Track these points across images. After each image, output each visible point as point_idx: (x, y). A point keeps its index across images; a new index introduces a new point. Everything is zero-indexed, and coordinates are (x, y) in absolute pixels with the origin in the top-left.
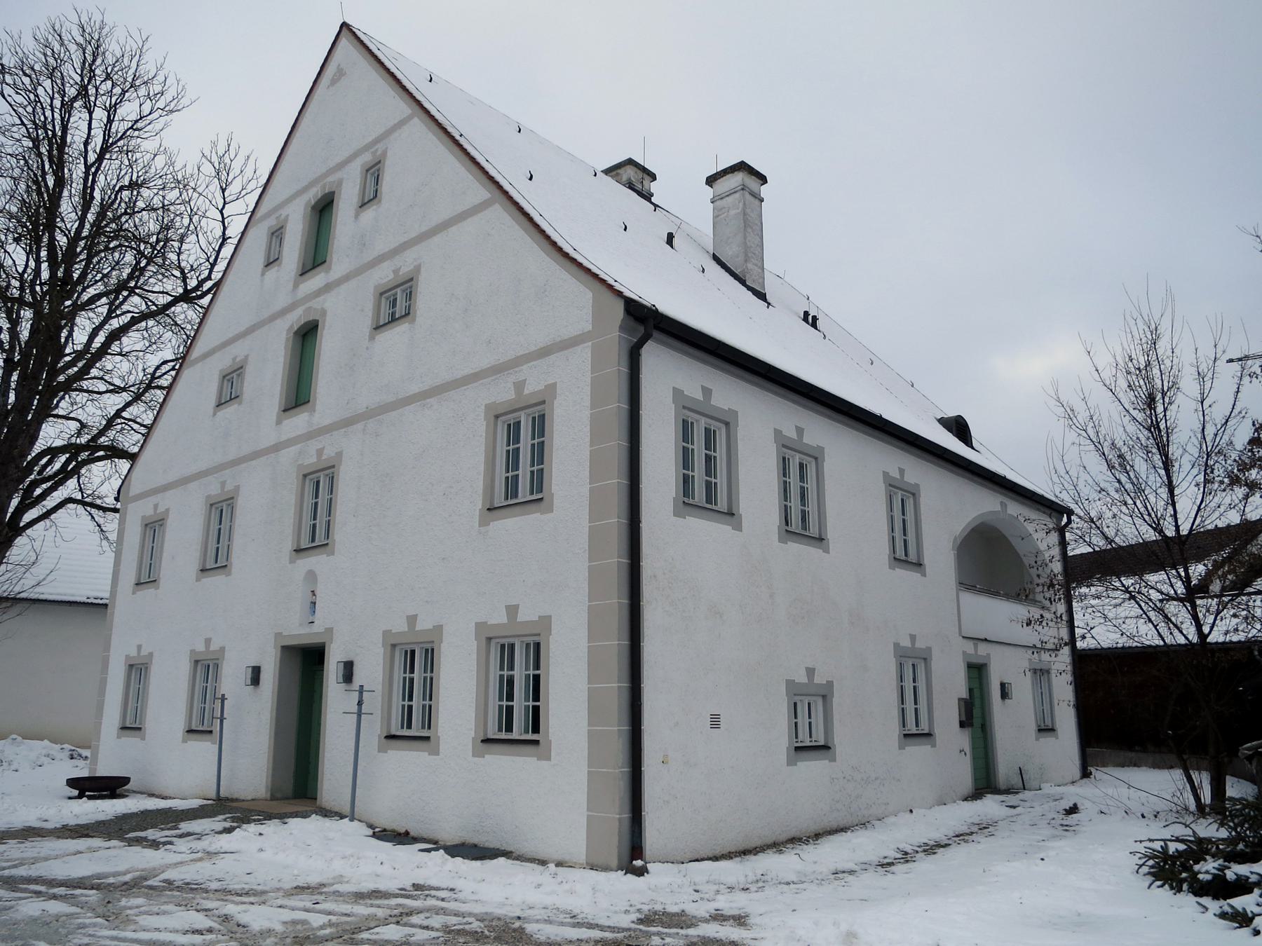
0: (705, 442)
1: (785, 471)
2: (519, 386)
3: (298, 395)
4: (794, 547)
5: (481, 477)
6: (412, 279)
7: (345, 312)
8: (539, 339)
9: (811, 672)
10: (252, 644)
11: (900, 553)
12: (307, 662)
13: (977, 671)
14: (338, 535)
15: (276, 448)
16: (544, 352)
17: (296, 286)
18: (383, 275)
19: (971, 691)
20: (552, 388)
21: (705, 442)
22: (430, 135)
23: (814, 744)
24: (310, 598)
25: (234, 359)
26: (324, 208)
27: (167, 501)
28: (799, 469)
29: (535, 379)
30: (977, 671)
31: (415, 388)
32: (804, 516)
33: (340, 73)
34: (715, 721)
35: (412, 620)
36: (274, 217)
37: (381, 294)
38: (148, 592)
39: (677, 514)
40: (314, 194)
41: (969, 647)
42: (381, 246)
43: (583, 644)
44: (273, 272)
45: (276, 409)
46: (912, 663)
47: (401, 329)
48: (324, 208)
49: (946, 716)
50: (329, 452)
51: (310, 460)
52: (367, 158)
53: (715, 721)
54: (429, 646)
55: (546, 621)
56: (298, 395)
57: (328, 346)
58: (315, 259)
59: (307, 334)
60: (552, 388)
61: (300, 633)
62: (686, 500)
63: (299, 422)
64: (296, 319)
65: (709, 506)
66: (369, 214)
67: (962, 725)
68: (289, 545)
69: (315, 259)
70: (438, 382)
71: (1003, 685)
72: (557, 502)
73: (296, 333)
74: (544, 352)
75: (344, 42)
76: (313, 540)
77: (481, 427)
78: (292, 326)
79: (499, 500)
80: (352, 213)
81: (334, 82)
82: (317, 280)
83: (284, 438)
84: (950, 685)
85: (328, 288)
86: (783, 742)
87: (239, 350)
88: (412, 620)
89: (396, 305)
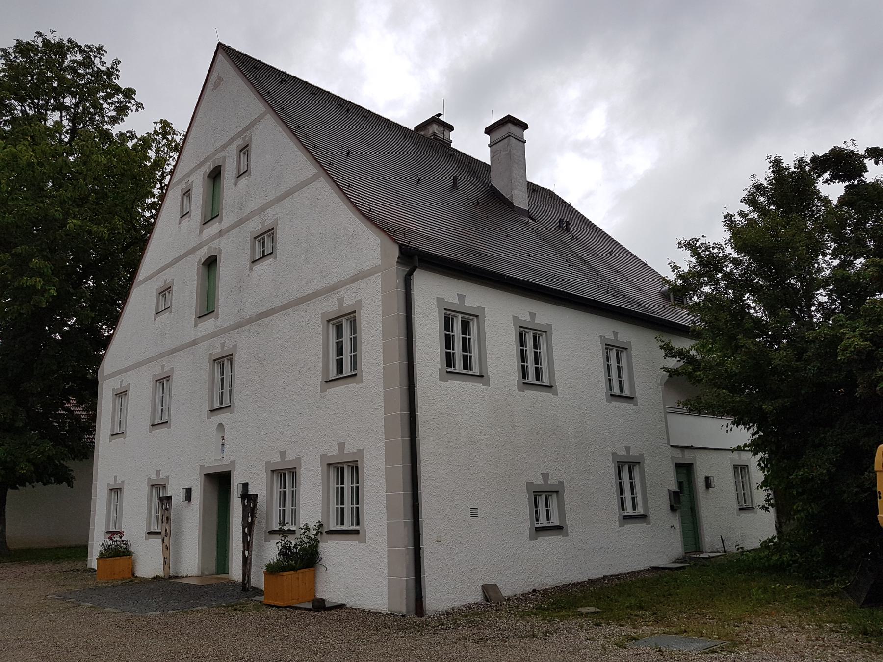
0: (458, 328)
1: (522, 342)
2: (341, 301)
3: (207, 308)
4: (530, 393)
5: (321, 361)
6: (273, 229)
7: (234, 253)
8: (349, 270)
9: (545, 476)
10: (186, 479)
11: (616, 390)
12: (220, 481)
13: (685, 470)
14: (237, 400)
15: (194, 343)
16: (355, 279)
17: (201, 232)
18: (255, 226)
19: (680, 484)
20: (359, 302)
21: (458, 328)
22: (278, 128)
23: (551, 525)
24: (221, 442)
25: (165, 281)
26: (215, 175)
27: (129, 379)
28: (530, 339)
29: (349, 298)
30: (685, 470)
31: (278, 302)
32: (538, 372)
33: (220, 79)
34: (474, 513)
35: (283, 454)
36: (184, 182)
37: (255, 238)
38: (119, 440)
39: (442, 379)
40: (208, 167)
41: (678, 454)
42: (253, 205)
43: (383, 467)
44: (186, 220)
45: (199, 223)
46: (627, 466)
47: (269, 261)
48: (215, 175)
49: (659, 505)
50: (229, 345)
51: (217, 351)
52: (240, 142)
53: (474, 513)
54: (354, 464)
55: (361, 452)
56: (207, 308)
57: (224, 270)
58: (212, 215)
59: (211, 263)
60: (359, 302)
61: (215, 465)
62: (449, 369)
63: (209, 325)
64: (203, 254)
65: (465, 372)
66: (244, 181)
67: (673, 509)
68: (206, 408)
69: (212, 215)
70: (292, 298)
71: (707, 479)
72: (365, 376)
73: (208, 176)
74: (355, 279)
75: (220, 57)
76: (222, 403)
77: (319, 328)
78: (200, 259)
79: (333, 375)
80: (233, 181)
81: (216, 86)
82: (214, 228)
83: (200, 335)
84: (661, 479)
85: (221, 234)
86: (525, 524)
87: (167, 275)
88: (283, 454)
89: (265, 243)
